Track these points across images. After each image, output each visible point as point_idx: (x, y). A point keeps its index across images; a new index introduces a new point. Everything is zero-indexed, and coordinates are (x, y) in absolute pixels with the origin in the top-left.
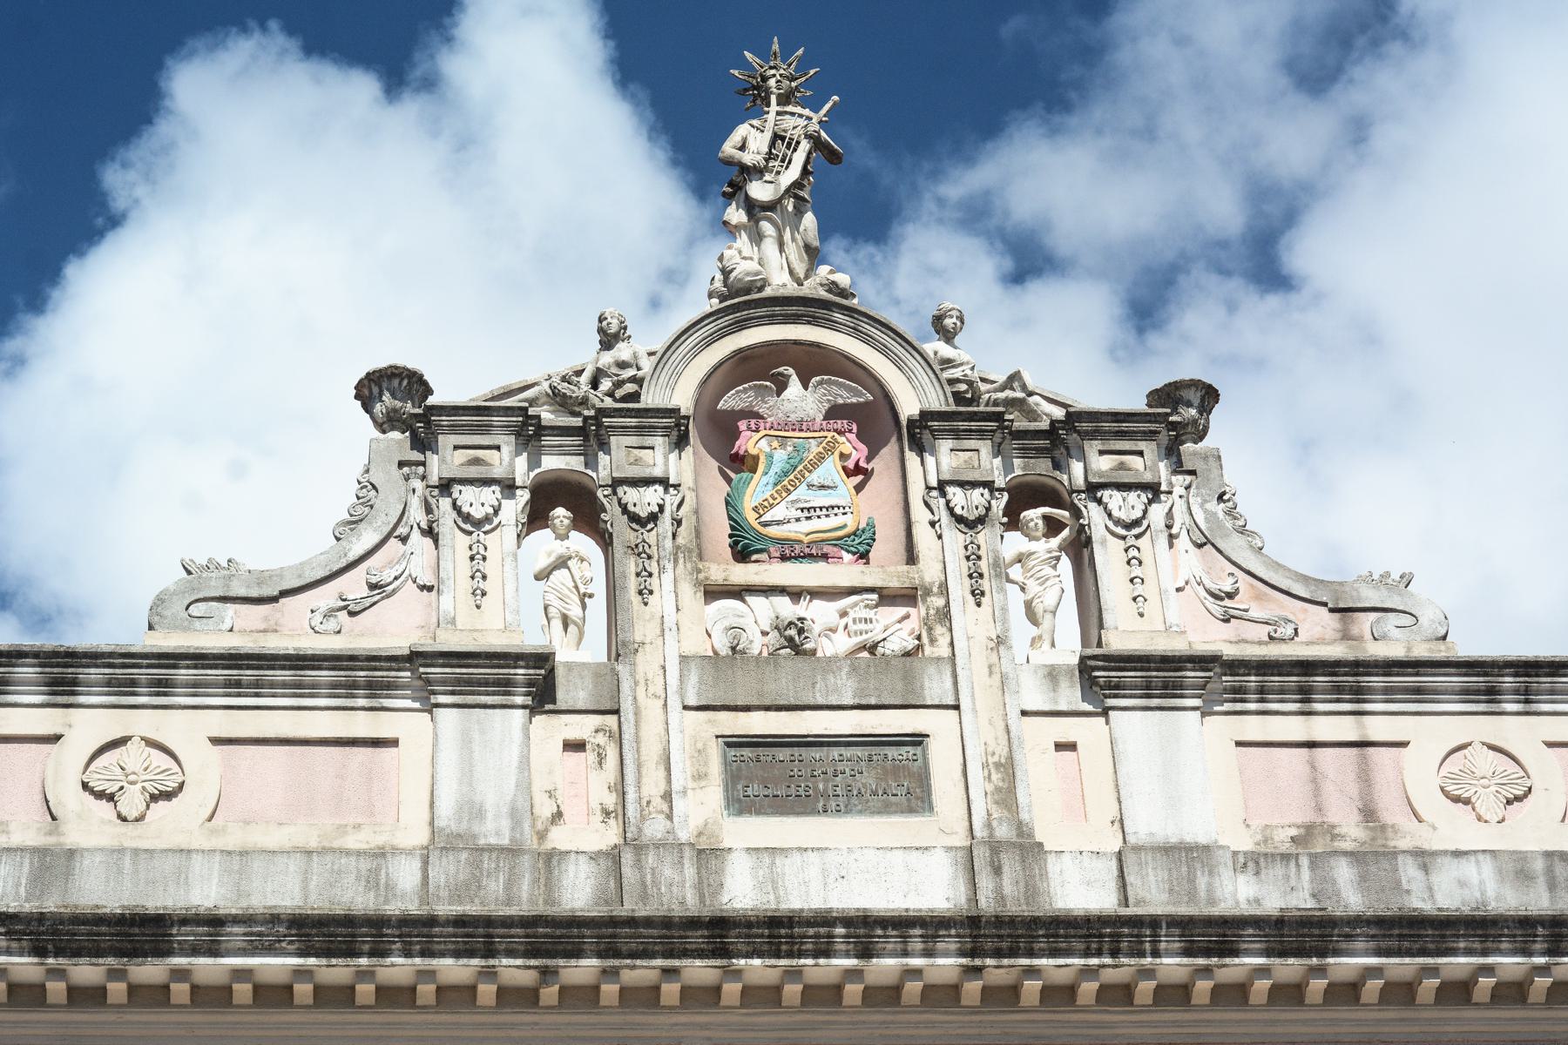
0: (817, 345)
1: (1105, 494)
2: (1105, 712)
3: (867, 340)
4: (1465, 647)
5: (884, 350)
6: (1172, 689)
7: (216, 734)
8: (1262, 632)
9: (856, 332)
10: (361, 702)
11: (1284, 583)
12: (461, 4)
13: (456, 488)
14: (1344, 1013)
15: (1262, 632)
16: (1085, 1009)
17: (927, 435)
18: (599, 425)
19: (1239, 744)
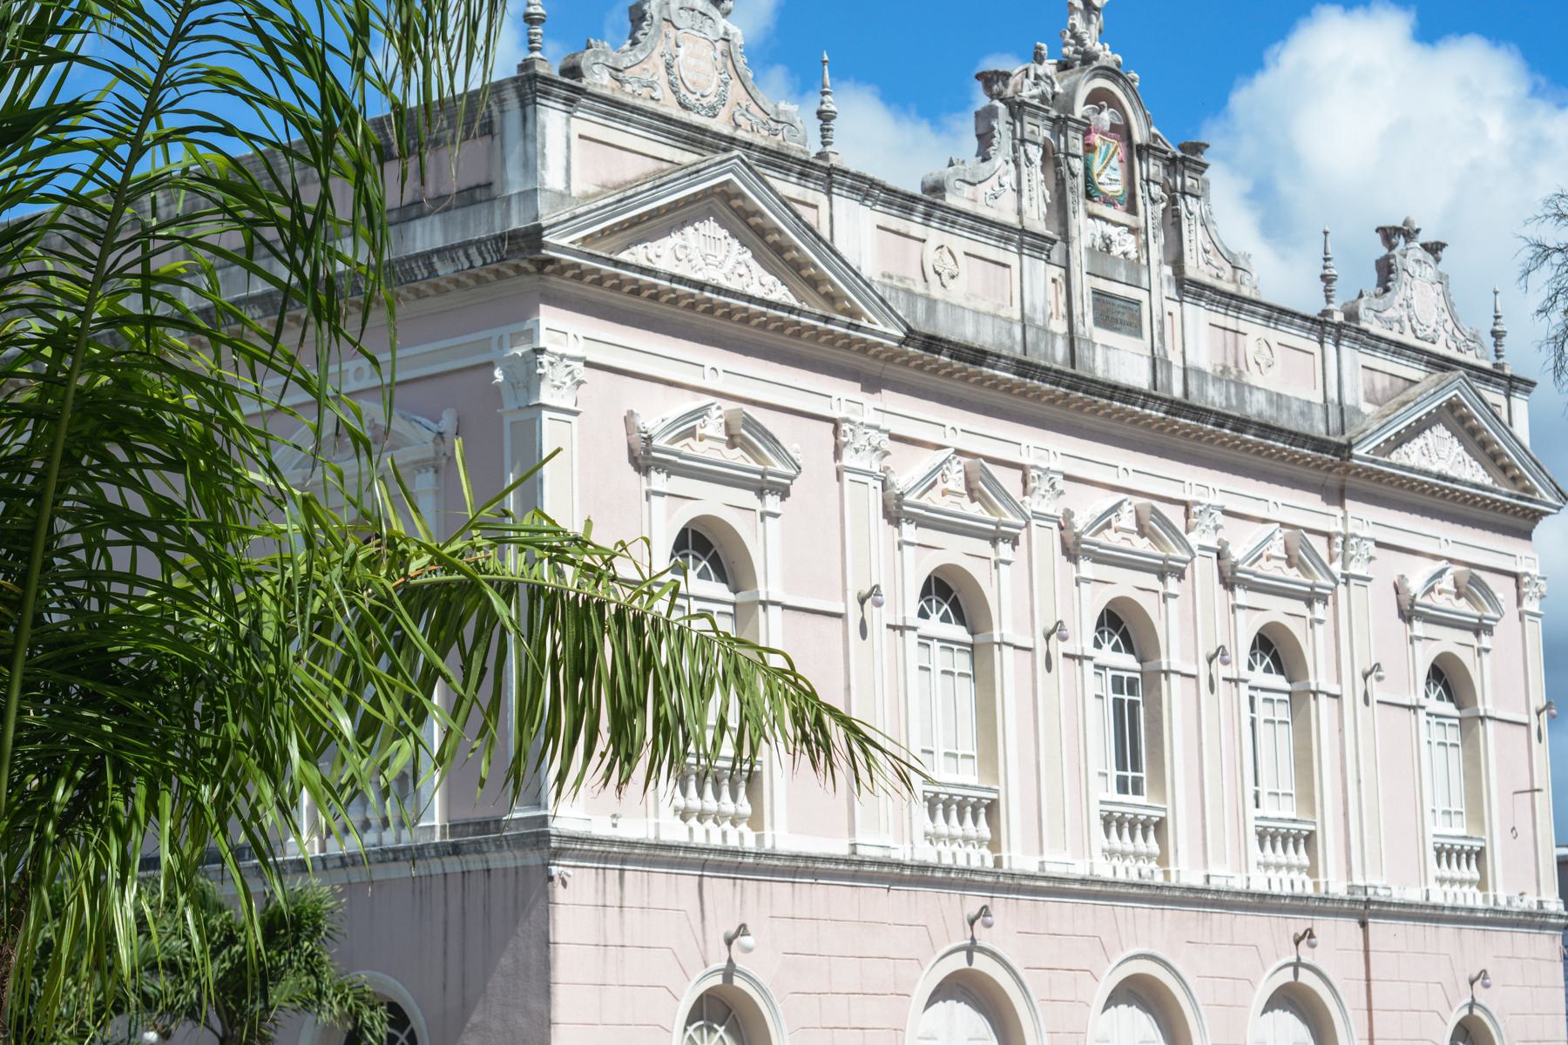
0: (1112, 93)
1: (1027, 144)
2: (1181, 301)
3: (1127, 95)
4: (1265, 299)
5: (1131, 102)
6: (867, 196)
7: (882, 224)
8: (1215, 272)
9: (1124, 90)
10: (993, 242)
11: (1222, 251)
12: (1561, 106)
13: (1027, 144)
14: (634, 299)
15: (1215, 272)
16: (819, 344)
17: (1145, 154)
18: (1065, 122)
19: (879, 227)
